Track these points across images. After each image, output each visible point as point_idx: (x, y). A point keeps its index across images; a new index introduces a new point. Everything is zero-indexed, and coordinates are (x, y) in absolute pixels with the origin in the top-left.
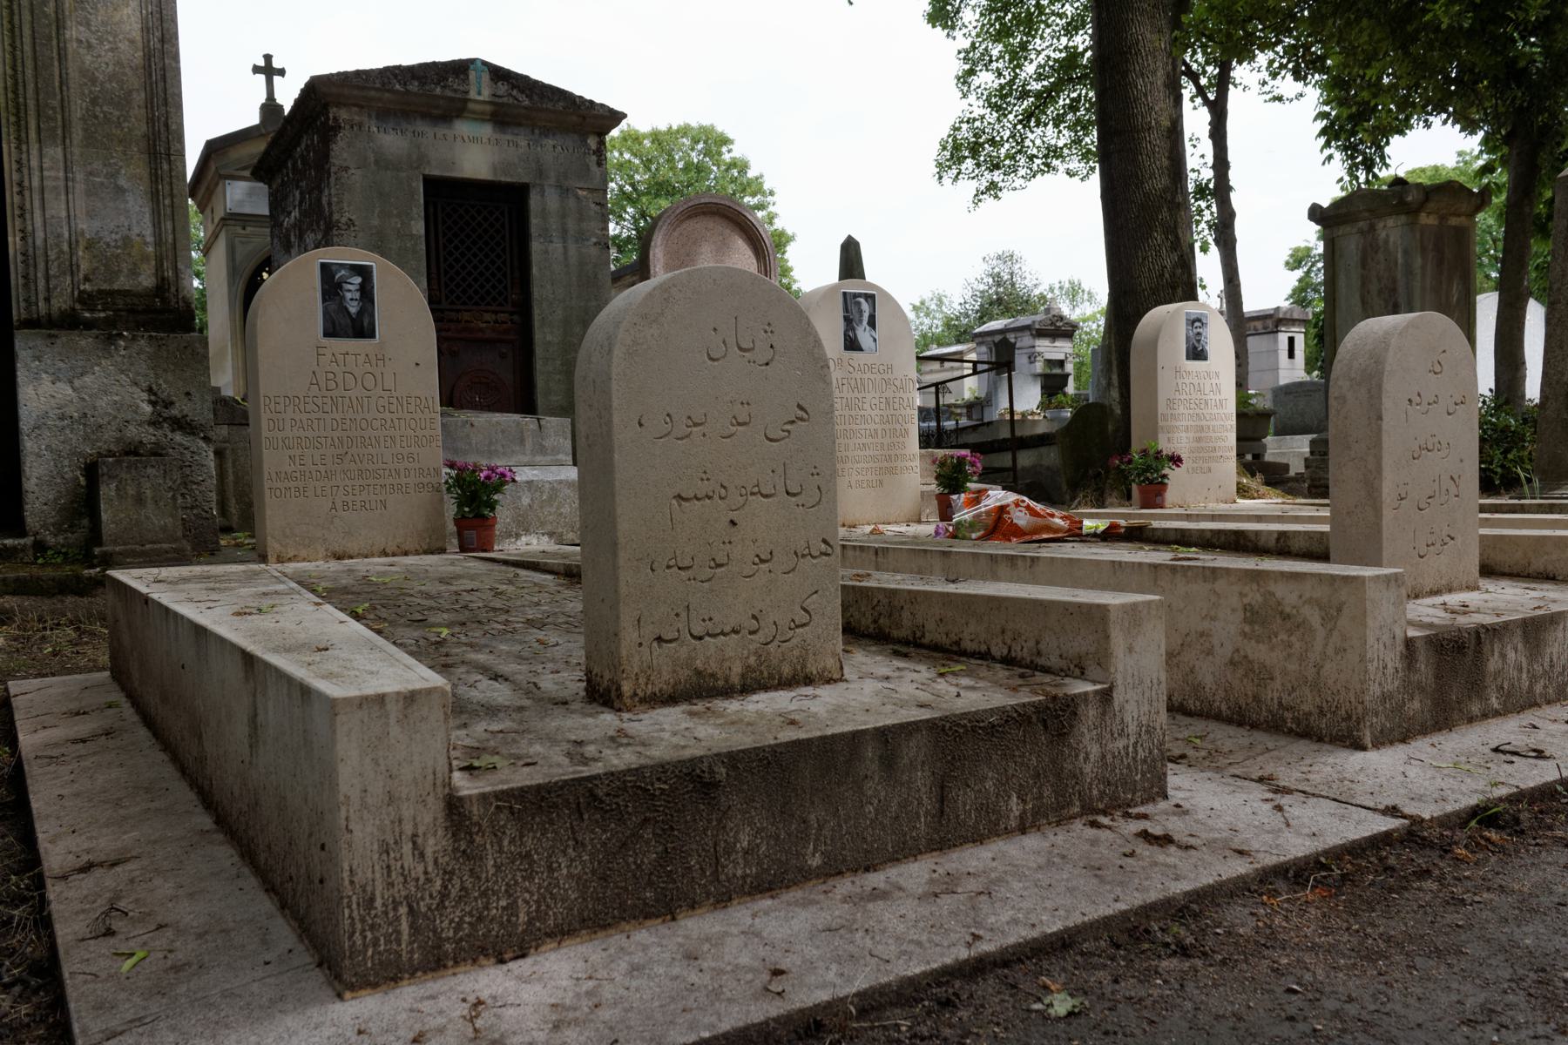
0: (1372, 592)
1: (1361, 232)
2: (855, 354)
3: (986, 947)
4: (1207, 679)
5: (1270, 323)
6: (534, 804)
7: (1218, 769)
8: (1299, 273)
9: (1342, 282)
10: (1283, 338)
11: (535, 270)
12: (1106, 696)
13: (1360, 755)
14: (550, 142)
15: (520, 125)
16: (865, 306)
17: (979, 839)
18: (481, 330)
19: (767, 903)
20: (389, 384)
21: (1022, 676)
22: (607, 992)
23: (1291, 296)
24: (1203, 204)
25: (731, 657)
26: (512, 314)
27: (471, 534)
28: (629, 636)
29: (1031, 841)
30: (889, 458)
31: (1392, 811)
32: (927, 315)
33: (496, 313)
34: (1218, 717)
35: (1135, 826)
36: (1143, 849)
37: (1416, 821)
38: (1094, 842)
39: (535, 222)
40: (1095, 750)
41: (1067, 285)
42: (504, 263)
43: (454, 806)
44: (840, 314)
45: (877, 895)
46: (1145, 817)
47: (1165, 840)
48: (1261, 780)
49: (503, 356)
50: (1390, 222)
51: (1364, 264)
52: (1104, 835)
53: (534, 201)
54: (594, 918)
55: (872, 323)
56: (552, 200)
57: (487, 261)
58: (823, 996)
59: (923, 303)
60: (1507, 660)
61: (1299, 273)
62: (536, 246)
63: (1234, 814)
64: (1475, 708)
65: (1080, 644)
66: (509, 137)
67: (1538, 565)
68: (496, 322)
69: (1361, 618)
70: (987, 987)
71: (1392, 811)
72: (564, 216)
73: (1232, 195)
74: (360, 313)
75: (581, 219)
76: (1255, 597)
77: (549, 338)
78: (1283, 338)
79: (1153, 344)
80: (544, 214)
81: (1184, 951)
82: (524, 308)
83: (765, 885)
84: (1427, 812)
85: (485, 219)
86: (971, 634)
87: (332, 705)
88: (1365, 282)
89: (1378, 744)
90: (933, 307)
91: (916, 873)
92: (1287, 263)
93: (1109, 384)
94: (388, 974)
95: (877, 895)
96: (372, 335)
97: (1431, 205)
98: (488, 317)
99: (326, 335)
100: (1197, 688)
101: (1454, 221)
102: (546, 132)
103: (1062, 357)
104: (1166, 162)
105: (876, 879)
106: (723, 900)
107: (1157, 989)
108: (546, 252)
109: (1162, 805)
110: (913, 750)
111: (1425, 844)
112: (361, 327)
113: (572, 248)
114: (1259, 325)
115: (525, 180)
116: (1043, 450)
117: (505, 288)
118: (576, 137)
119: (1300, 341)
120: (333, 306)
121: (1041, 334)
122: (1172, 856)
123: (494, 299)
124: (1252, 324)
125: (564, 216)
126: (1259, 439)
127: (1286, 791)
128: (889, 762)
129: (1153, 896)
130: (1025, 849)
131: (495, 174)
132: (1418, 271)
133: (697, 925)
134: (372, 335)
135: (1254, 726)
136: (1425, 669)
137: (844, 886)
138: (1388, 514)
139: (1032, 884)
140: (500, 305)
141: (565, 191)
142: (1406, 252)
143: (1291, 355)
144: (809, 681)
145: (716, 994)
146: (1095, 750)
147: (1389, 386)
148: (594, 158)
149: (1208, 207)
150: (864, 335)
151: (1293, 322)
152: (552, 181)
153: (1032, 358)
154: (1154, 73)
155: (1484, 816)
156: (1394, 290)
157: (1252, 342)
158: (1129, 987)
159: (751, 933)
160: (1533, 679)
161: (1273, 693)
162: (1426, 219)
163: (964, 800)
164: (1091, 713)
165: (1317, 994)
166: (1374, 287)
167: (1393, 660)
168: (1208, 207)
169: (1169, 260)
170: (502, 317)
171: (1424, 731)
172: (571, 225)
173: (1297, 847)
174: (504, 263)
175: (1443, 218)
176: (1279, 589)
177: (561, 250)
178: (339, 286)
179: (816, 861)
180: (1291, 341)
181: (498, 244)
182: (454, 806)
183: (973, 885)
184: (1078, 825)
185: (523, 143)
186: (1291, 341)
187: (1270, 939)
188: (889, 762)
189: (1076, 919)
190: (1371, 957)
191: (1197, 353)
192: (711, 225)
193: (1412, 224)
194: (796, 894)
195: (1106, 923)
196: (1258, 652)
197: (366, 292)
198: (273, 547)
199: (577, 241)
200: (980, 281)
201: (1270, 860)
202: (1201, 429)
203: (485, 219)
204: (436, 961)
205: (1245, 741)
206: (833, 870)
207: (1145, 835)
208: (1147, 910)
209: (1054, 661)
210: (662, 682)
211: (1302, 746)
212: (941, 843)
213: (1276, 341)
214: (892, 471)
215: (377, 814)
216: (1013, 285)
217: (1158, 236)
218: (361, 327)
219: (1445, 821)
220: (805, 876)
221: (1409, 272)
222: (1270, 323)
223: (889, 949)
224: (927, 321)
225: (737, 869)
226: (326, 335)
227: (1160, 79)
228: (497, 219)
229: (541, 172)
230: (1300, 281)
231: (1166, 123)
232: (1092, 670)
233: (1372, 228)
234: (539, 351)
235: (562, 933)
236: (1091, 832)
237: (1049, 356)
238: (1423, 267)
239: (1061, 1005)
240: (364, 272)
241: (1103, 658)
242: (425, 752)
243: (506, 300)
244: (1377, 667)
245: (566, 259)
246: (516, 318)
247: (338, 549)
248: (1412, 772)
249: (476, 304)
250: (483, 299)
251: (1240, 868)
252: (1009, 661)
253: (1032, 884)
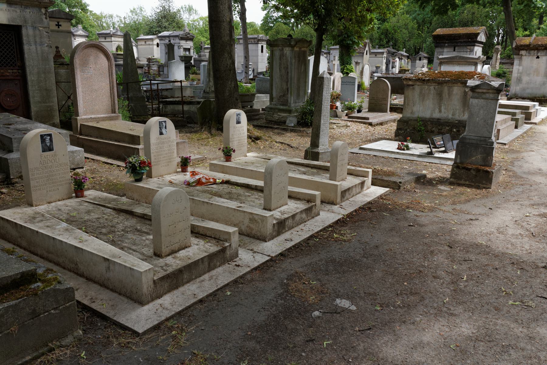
0: (268, 218)
1: (280, 50)
2: (162, 136)
3: (219, 287)
4: (243, 229)
5: (256, 40)
6: (162, 279)
7: (245, 248)
8: (266, 12)
9: (274, 63)
10: (260, 46)
11: (26, 56)
12: (230, 245)
13: (266, 243)
14: (28, 11)
15: (17, 4)
16: (164, 124)
17: (214, 269)
18: (8, 76)
19: (188, 284)
20: (57, 160)
21: (218, 242)
22: (176, 301)
23: (263, 20)
24: (236, 5)
25: (176, 246)
26: (18, 70)
27: (79, 194)
28: (163, 247)
29: (221, 268)
30: (170, 159)
31: (269, 256)
32: (136, 15)
33: (12, 70)
34: (245, 235)
35: (235, 263)
36: (236, 268)
37: (272, 257)
38: (229, 267)
39: (25, 39)
40: (229, 253)
41: (188, 7)
42: (14, 52)
43: (154, 281)
44: (158, 126)
45: (203, 281)
46: (235, 261)
47: (238, 266)
48: (251, 250)
49: (16, 84)
50: (287, 49)
51: (280, 59)
52: (230, 266)
53: (24, 31)
54: (169, 291)
55: (166, 128)
56: (31, 31)
57: (8, 52)
58: (201, 297)
59: (134, 9)
60: (289, 222)
61: (266, 12)
62: (26, 47)
63: (249, 258)
64: (284, 231)
65: (226, 237)
66: (13, 9)
67: (298, 197)
68: (13, 73)
69: (267, 223)
70: (219, 292)
71: (269, 256)
72: (35, 37)
73: (245, 3)
74: (50, 145)
75: (41, 38)
76: (251, 217)
77: (33, 78)
78: (260, 46)
79: (229, 121)
80: (28, 36)
81: (242, 284)
82: (23, 68)
83: (188, 282)
84: (273, 255)
85: (6, 37)
86: (208, 233)
87: (141, 273)
88: (280, 64)
89: (269, 241)
90: (138, 11)
91: (206, 276)
92: (262, 8)
93: (209, 81)
94: (148, 303)
95: (203, 281)
96: (53, 150)
97: (297, 45)
98: (9, 71)
99: (43, 152)
100: (241, 230)
101: (303, 49)
102: (27, 7)
103: (189, 47)
104: (228, 32)
105: (202, 278)
106: (183, 285)
107: (240, 289)
108: (30, 49)
109: (238, 258)
110: (205, 260)
111: (273, 261)
112: (50, 149)
113: (39, 48)
114: (253, 40)
115: (20, 24)
116: (191, 106)
117: (15, 61)
118: (37, 9)
119: (265, 46)
120: (44, 145)
121: (182, 39)
122: (240, 268)
123: (11, 65)
124: (251, 40)
125: (35, 37)
126: (252, 102)
127: (255, 252)
128: (202, 262)
129: (238, 276)
130: (220, 270)
131: (9, 22)
132: (293, 64)
133: (181, 289)
134: (53, 150)
135: (251, 237)
136: (276, 228)
137: (198, 280)
138: (273, 196)
139: (222, 275)
140: (14, 67)
141: (35, 28)
142: (291, 58)
143: (262, 52)
144: (186, 247)
145: (189, 298)
146: (229, 253)
147: (273, 175)
148: (44, 16)
149: (238, 6)
150: (164, 131)
151: (263, 40)
152: (30, 24)
153: (179, 47)
154: (225, 4)
155: (281, 254)
156: (287, 68)
157: (251, 47)
158: (236, 290)
159: (189, 289)
160: (293, 224)
161: (254, 232)
162: (296, 49)
163: (212, 264)
164: (228, 248)
165: (257, 287)
166: (283, 66)
167: (271, 227)
168: (238, 6)
169: (229, 62)
170: (15, 71)
171: (276, 237)
172: (38, 40)
173: (256, 264)
174: (13, 48)
175: (300, 48)
176: (255, 216)
177: (35, 48)
178: (45, 140)
179: (194, 277)
180: (262, 46)
181: (11, 46)
182: (154, 281)
183: (214, 277)
184: (226, 264)
185: (18, 11)
186: (262, 46)
187: (252, 280)
188: (202, 262)
189: (229, 281)
190: (264, 281)
191: (238, 122)
192: (93, 50)
193: (292, 50)
194: (192, 282)
195: (232, 281)
196: (252, 226)
197: (51, 140)
198: (34, 203)
199: (40, 45)
200: (158, 8)
201: (252, 267)
202: (239, 140)
203: (6, 37)
204: (153, 300)
205: (249, 241)
206: (196, 278)
207: (236, 265)
208: (237, 278)
209: (222, 239)
210: (167, 253)
211: (258, 241)
212: (209, 271)
213: (258, 46)
214: (170, 162)
215: (146, 285)
216: (170, 11)
217: (226, 55)
218: (50, 149)
219: (276, 256)
220: (193, 279)
221: (291, 64)
222: (256, 40)
223: (207, 289)
224: (136, 17)
225: (185, 281)
226: (43, 152)
227: (227, 6)
228: (10, 37)
229: (25, 21)
230: (266, 15)
231: (228, 20)
232: (228, 241)
233: (282, 50)
234: (30, 83)
235: (166, 293)
236: (228, 265)
237: (185, 47)
238: (295, 62)
239: (229, 293)
240: (50, 135)
241: (230, 239)
242: (150, 275)
243: (16, 65)
244: (269, 228)
245: (37, 51)
246: (19, 71)
247: (48, 201)
248: (273, 246)
249: (5, 67)
250: (7, 65)
251: (249, 269)
252: (215, 238)
253: (222, 275)
